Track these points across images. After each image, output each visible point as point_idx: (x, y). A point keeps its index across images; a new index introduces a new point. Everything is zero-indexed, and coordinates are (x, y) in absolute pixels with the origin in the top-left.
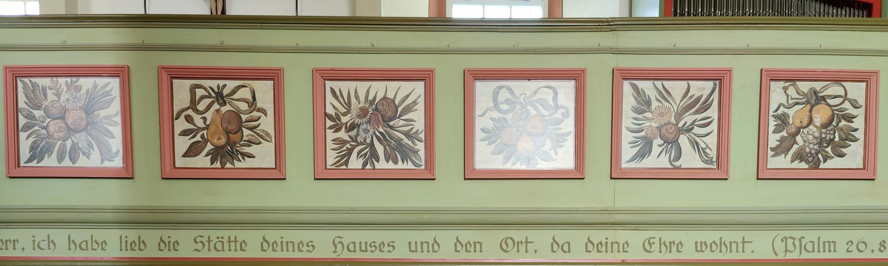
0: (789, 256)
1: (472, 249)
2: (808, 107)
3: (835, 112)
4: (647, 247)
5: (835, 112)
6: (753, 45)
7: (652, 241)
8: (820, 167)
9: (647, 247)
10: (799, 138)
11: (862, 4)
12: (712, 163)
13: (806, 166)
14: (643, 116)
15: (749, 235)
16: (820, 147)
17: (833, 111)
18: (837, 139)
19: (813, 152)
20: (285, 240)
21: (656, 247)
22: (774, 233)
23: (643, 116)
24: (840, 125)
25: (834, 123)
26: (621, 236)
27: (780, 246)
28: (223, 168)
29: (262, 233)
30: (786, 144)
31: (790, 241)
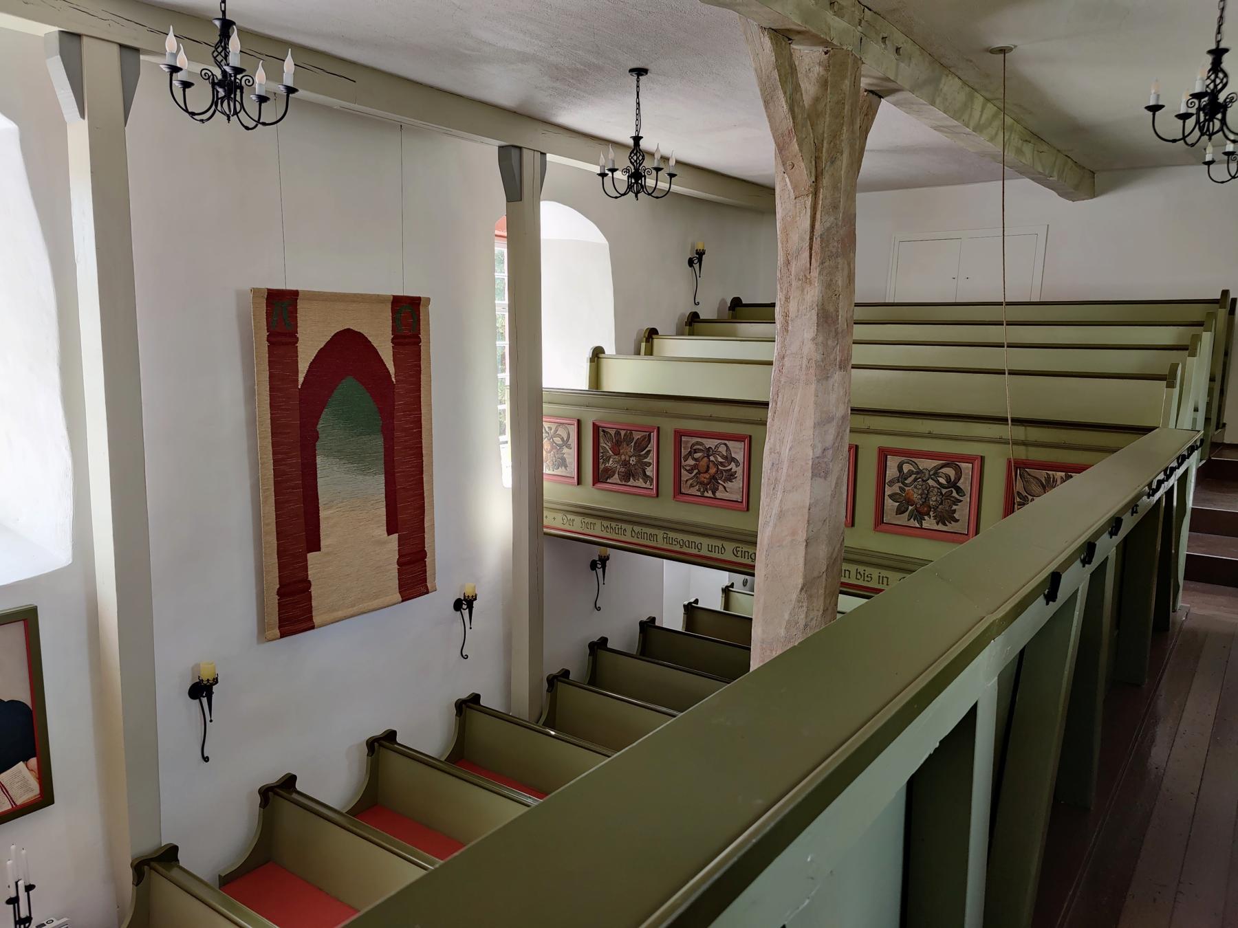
1: (589, 527)
4: (735, 552)
7: (738, 549)
9: (735, 552)
12: (650, 435)
20: (643, 531)
21: (739, 554)
26: (698, 540)
29: (879, 571)
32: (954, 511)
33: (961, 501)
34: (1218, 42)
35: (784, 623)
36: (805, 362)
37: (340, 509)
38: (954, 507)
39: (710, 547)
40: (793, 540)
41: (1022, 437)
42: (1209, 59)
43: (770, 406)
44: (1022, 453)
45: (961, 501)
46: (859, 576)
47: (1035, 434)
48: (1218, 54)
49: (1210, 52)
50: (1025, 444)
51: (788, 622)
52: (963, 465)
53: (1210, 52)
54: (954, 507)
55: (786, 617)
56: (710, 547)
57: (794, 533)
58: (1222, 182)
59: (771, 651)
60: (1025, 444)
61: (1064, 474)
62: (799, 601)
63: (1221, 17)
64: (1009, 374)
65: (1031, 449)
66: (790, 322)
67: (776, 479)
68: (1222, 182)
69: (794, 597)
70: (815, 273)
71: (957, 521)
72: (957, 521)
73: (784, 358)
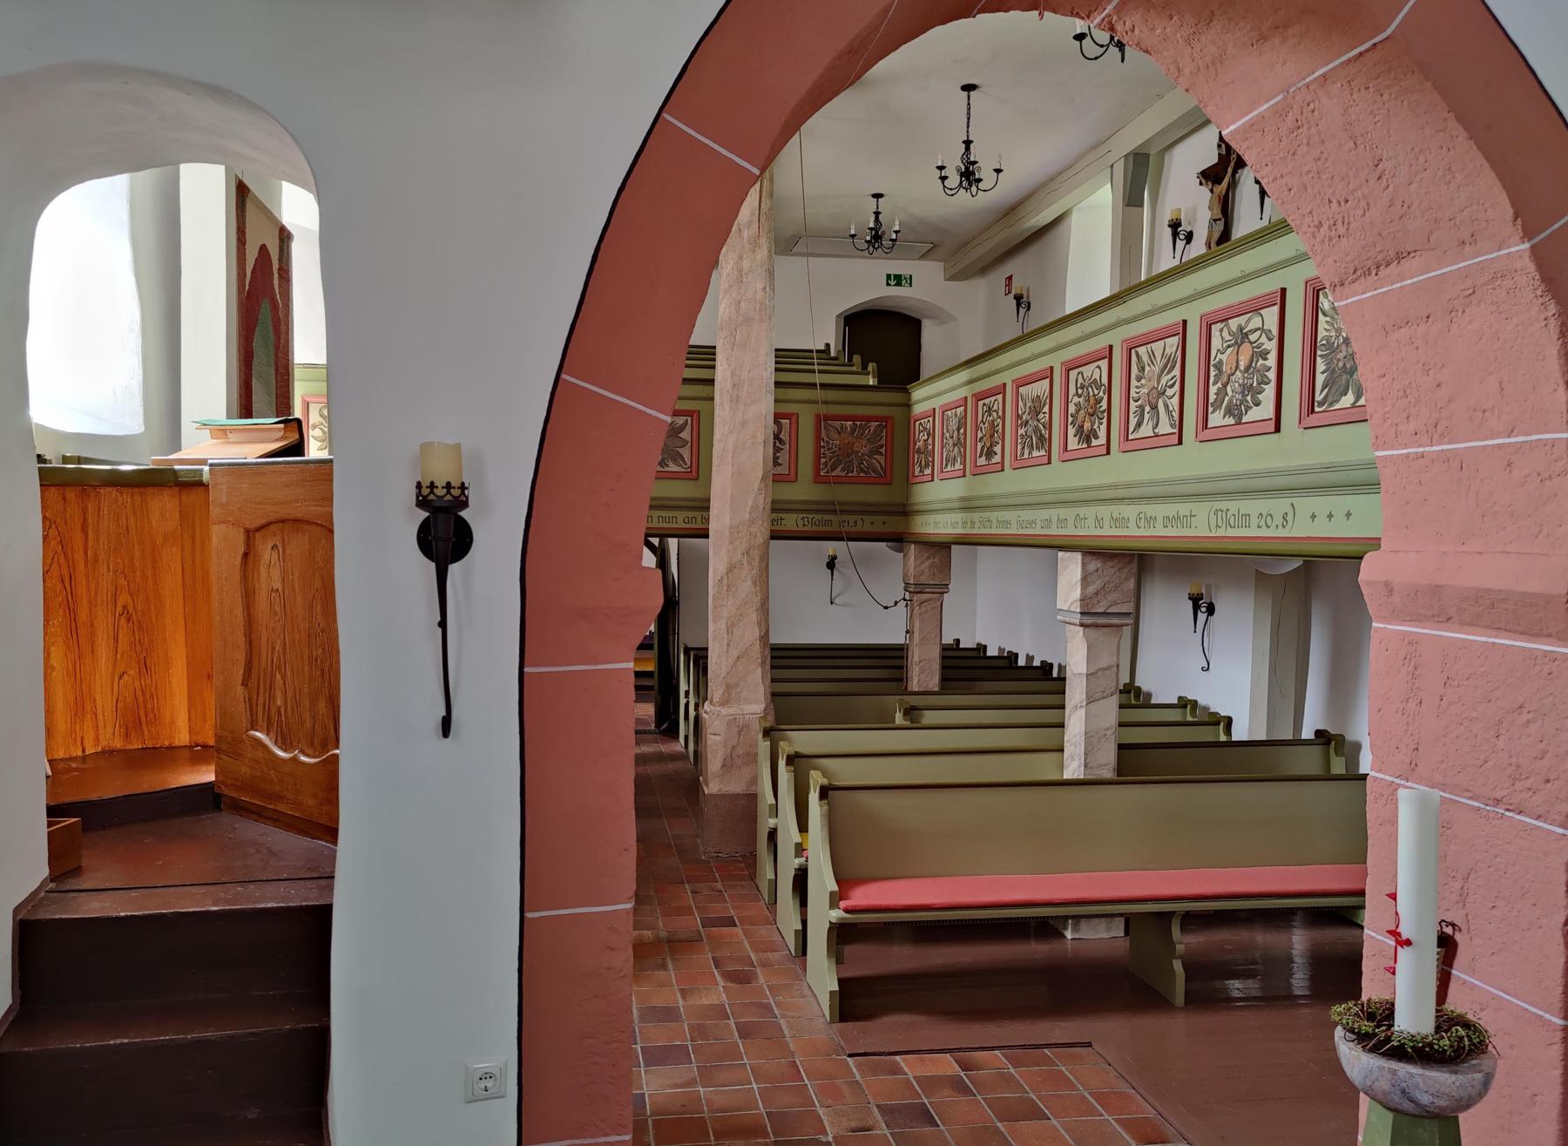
0: (806, 528)
2: (1236, 348)
3: (1255, 350)
5: (1255, 350)
6: (1200, 288)
8: (1243, 421)
10: (1229, 388)
11: (286, 377)
13: (1233, 422)
14: (1322, 373)
15: (784, 516)
16: (1243, 396)
17: (1253, 348)
18: (1255, 384)
19: (1238, 403)
22: (796, 515)
23: (1322, 373)
24: (1259, 364)
25: (1253, 365)
27: (800, 523)
28: (1089, 447)
30: (1221, 396)
31: (806, 519)
32: (778, 457)
33: (782, 449)
34: (968, 136)
35: (749, 509)
36: (758, 305)
37: (141, 705)
38: (778, 454)
39: (674, 521)
40: (753, 443)
41: (824, 399)
42: (964, 146)
43: (720, 357)
44: (823, 409)
45: (782, 449)
46: (704, 521)
47: (832, 395)
48: (968, 143)
49: (964, 142)
50: (825, 402)
51: (752, 507)
52: (783, 421)
53: (964, 142)
54: (778, 454)
55: (750, 503)
56: (674, 521)
57: (754, 437)
58: (1096, 58)
59: (738, 533)
60: (825, 402)
61: (851, 423)
62: (760, 490)
63: (968, 127)
64: (815, 385)
65: (830, 406)
66: (744, 275)
67: (737, 396)
68: (1096, 58)
69: (756, 486)
70: (763, 241)
71: (781, 465)
72: (781, 465)
73: (740, 302)
